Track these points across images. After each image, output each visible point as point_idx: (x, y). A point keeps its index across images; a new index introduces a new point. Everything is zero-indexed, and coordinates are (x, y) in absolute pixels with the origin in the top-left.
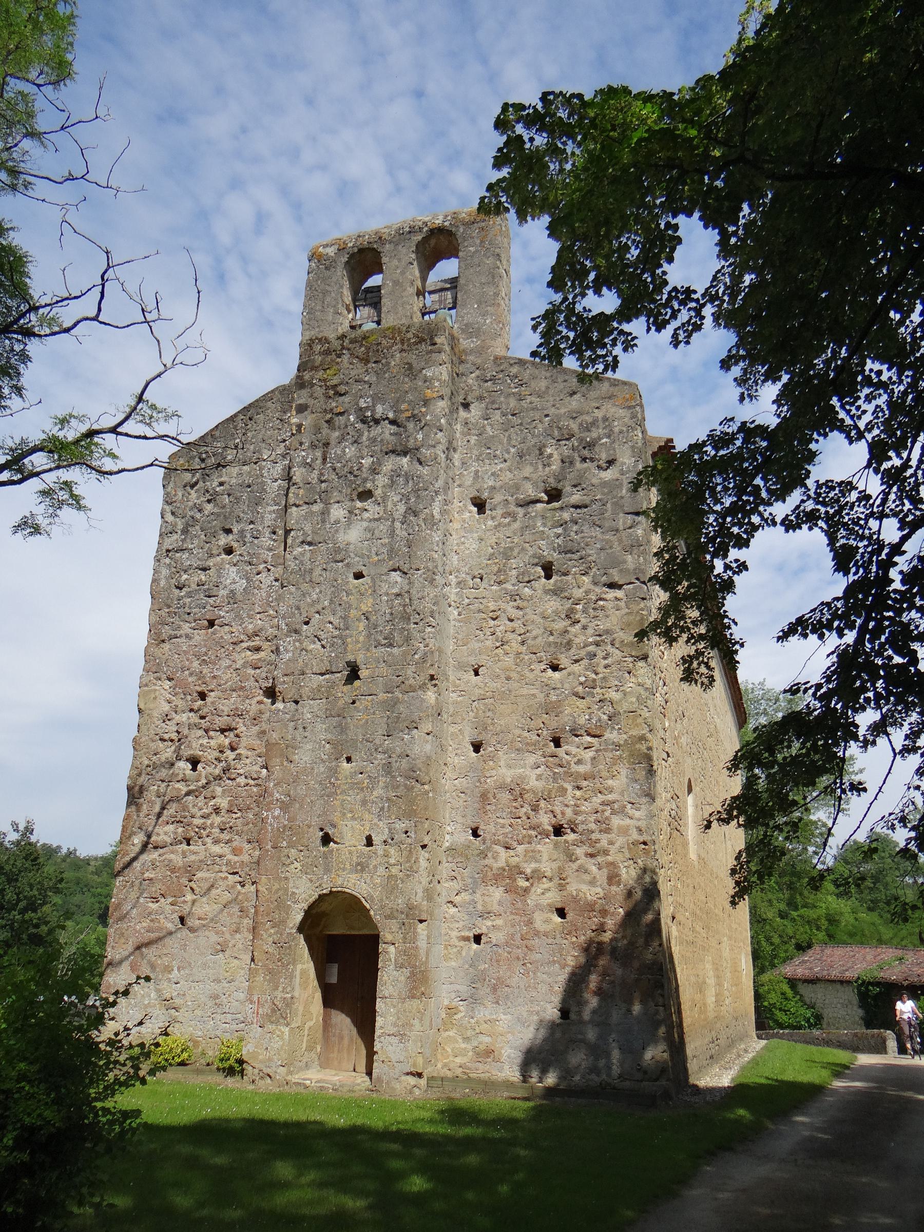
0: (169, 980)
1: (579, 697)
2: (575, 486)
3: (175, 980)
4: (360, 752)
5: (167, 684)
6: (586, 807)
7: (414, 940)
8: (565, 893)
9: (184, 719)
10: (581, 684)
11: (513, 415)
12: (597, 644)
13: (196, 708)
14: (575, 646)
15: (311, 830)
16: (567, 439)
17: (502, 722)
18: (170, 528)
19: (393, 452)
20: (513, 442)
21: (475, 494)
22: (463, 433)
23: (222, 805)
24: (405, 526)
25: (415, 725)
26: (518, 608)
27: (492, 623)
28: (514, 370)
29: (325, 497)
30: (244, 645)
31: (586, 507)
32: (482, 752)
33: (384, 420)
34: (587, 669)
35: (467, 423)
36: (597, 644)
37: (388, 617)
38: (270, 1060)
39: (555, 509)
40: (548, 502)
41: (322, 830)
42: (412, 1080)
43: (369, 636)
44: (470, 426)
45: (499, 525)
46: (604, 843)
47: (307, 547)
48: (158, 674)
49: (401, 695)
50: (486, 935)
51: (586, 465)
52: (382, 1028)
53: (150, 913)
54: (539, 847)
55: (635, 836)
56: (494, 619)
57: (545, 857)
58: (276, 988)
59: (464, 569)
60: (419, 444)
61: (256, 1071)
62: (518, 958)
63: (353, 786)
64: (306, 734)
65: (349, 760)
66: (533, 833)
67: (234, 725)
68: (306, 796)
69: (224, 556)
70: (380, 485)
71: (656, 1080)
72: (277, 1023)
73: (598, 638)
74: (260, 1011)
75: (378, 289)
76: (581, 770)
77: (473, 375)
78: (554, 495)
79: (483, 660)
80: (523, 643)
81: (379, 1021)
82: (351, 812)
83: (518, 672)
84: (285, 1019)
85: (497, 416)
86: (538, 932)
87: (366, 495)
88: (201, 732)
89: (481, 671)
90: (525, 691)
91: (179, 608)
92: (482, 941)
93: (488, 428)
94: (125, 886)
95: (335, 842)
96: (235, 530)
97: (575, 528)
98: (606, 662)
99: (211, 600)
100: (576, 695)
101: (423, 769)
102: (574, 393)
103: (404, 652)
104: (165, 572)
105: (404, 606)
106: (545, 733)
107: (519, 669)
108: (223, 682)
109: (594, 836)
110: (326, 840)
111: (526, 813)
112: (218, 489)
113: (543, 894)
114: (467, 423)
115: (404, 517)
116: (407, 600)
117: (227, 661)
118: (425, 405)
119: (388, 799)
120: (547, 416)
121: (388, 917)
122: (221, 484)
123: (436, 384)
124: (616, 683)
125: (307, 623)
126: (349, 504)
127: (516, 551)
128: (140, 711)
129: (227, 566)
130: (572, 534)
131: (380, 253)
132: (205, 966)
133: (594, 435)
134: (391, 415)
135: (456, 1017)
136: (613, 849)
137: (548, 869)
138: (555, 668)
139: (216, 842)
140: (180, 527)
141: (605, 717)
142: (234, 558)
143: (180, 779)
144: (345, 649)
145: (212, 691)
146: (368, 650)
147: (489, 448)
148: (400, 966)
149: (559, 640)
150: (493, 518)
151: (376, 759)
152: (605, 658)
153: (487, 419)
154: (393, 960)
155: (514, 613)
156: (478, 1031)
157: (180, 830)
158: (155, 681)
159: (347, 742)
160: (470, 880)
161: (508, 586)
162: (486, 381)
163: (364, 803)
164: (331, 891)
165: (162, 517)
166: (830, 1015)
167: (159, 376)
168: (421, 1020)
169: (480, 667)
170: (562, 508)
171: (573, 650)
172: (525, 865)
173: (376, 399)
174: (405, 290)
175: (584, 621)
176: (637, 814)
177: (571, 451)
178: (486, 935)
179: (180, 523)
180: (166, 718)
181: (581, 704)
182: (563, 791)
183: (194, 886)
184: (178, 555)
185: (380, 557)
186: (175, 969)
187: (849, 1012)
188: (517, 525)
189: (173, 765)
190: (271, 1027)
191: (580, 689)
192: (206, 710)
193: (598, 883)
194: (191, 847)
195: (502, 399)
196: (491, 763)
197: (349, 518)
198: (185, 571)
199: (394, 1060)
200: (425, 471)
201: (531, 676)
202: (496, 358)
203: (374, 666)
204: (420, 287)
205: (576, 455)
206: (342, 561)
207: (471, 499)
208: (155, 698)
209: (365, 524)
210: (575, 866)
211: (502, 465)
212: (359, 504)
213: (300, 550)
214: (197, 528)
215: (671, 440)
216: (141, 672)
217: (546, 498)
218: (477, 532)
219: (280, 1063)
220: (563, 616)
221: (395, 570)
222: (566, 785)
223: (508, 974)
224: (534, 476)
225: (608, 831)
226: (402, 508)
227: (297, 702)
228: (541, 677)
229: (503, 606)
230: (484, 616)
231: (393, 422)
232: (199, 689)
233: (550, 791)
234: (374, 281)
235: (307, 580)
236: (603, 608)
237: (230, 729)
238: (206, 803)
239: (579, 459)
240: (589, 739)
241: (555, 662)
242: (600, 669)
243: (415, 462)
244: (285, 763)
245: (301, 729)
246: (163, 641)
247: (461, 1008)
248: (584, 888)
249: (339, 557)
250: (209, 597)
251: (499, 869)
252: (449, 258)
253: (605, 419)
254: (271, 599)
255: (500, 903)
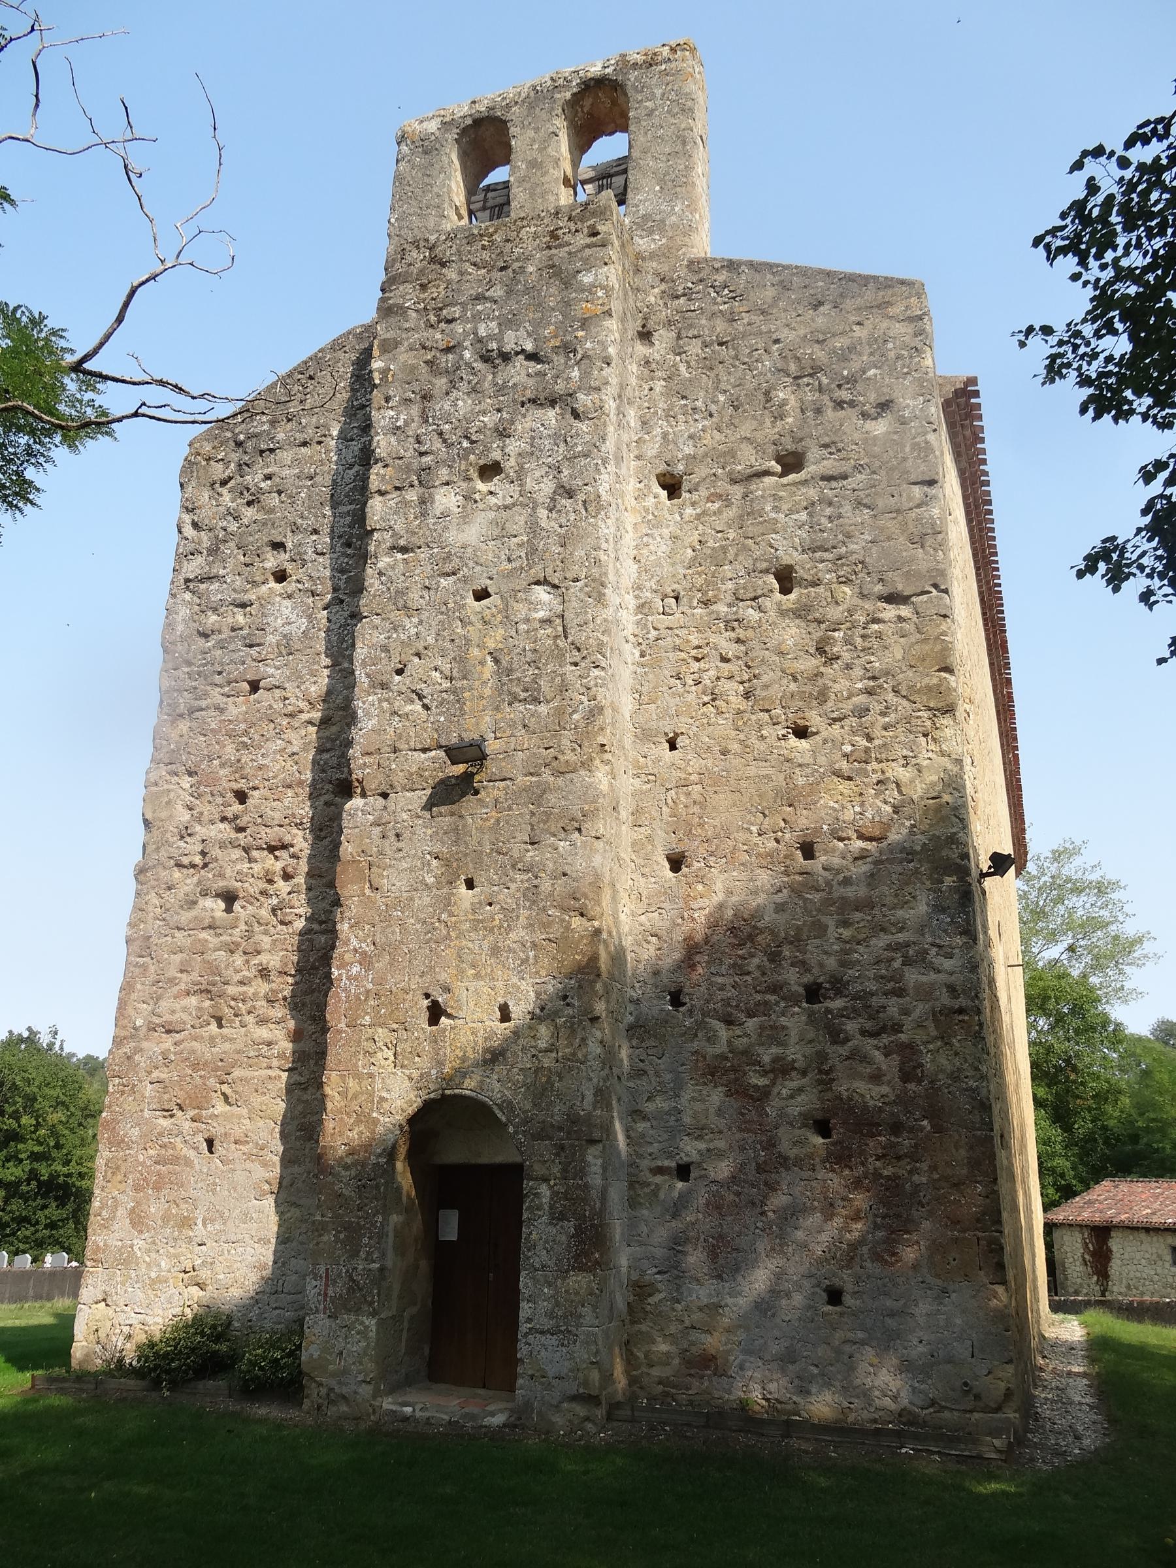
0: (190, 1240)
1: (843, 777)
2: (826, 446)
3: (199, 1240)
4: (487, 871)
5: (186, 782)
6: (860, 954)
7: (581, 1173)
8: (829, 1095)
9: (212, 834)
10: (846, 756)
11: (721, 344)
12: (870, 692)
13: (230, 815)
14: (833, 696)
15: (410, 997)
16: (810, 375)
17: (716, 822)
18: (191, 547)
19: (533, 401)
20: (723, 386)
21: (662, 468)
22: (641, 378)
23: (272, 963)
24: (554, 515)
25: (576, 825)
26: (738, 641)
27: (695, 666)
28: (721, 278)
29: (424, 478)
30: (305, 717)
31: (845, 477)
32: (684, 870)
33: (517, 353)
34: (853, 732)
35: (647, 362)
36: (870, 692)
37: (530, 656)
38: (345, 1372)
39: (794, 484)
40: (781, 476)
41: (427, 996)
42: (581, 1410)
43: (499, 690)
44: (654, 366)
45: (704, 513)
46: (893, 1010)
47: (399, 556)
48: (173, 767)
49: (552, 779)
50: (699, 1165)
51: (841, 414)
52: (529, 1320)
53: (160, 1134)
54: (784, 1021)
55: (945, 1000)
56: (697, 660)
57: (794, 1037)
58: (354, 1254)
59: (648, 585)
60: (572, 386)
61: (323, 1391)
62: (753, 1204)
63: (476, 925)
64: (400, 845)
65: (470, 884)
66: (772, 998)
67: (287, 839)
68: (402, 942)
69: (272, 584)
70: (512, 454)
71: (998, 1409)
72: (358, 1311)
73: (872, 683)
74: (330, 1292)
75: (506, 185)
76: (850, 895)
77: (656, 290)
78: (791, 462)
79: (682, 724)
80: (747, 695)
81: (525, 1309)
82: (474, 966)
83: (741, 742)
84: (371, 1304)
85: (694, 348)
86: (786, 1158)
87: (490, 470)
88: (237, 853)
89: (680, 743)
90: (752, 771)
91: (205, 665)
92: (692, 1175)
93: (683, 368)
94: (123, 1093)
95: (449, 1016)
96: (289, 545)
97: (828, 511)
98: (887, 719)
99: (253, 652)
100: (838, 774)
101: (591, 895)
102: (821, 303)
103: (557, 709)
104: (183, 612)
105: (556, 637)
106: (788, 836)
107: (742, 737)
108: (271, 774)
109: (875, 1001)
110: (436, 1012)
111: (759, 967)
112: (263, 485)
113: (792, 1097)
114: (647, 362)
115: (553, 500)
116: (560, 629)
117: (279, 742)
118: (583, 327)
119: (534, 945)
120: (777, 341)
121: (536, 1137)
122: (268, 477)
123: (600, 294)
124: (905, 752)
125: (400, 672)
126: (464, 485)
127: (732, 551)
128: (147, 823)
129: (278, 599)
130: (824, 521)
131: (505, 122)
132: (246, 1217)
133: (855, 366)
134: (529, 346)
135: (651, 1300)
136: (908, 1022)
137: (799, 1056)
138: (801, 732)
139: (262, 1021)
140: (206, 543)
141: (889, 809)
142: (290, 586)
143: (206, 925)
144: (461, 709)
145: (255, 788)
146: (497, 709)
147: (684, 397)
148: (558, 1217)
149: (808, 688)
150: (693, 504)
151: (513, 881)
152: (883, 714)
153: (679, 354)
154: (546, 1207)
155: (731, 649)
156: (687, 1323)
157: (208, 1003)
158: (168, 777)
159: (466, 855)
160: (669, 1076)
161: (722, 608)
162: (678, 297)
163: (495, 951)
164: (443, 1095)
165: (180, 532)
166: (1132, 1275)
167: (153, 277)
168: (595, 1307)
169: (677, 735)
170: (805, 482)
171: (830, 704)
172: (761, 1050)
173: (509, 322)
174: (547, 173)
175: (846, 656)
176: (948, 964)
177: (817, 394)
178: (699, 1165)
179: (205, 538)
180: (185, 833)
181: (844, 787)
182: (822, 930)
183: (228, 1091)
184: (203, 586)
185: (514, 564)
186: (199, 1222)
187: (1159, 1270)
188: (730, 513)
189: (195, 903)
190: (347, 1318)
191: (844, 765)
192: (246, 819)
193: (885, 1079)
194: (224, 1030)
195: (703, 322)
196: (700, 887)
197: (464, 507)
198: (215, 610)
199: (551, 1374)
200: (583, 426)
201: (760, 746)
202: (691, 262)
203: (508, 733)
204: (570, 173)
205: (826, 398)
206: (454, 574)
207: (658, 476)
208: (168, 803)
209: (492, 515)
210: (844, 1050)
211: (706, 423)
212: (481, 486)
213: (387, 560)
214: (232, 544)
215: (973, 381)
216: (148, 764)
217: (778, 469)
218: (668, 526)
219: (361, 1377)
220: (812, 650)
221: (538, 583)
222: (825, 919)
223: (737, 1229)
224: (759, 436)
225: (900, 993)
226: (548, 487)
227: (385, 796)
228: (777, 747)
229: (714, 638)
230: (683, 655)
231: (533, 357)
232: (235, 786)
233: (799, 929)
234: (498, 175)
235: (400, 605)
236: (879, 636)
237: (284, 847)
238: (247, 962)
239: (831, 404)
240: (860, 844)
241: (801, 722)
242: (878, 732)
243: (568, 416)
244: (368, 891)
245: (393, 838)
246: (181, 716)
247: (660, 1286)
248: (861, 1086)
249: (448, 568)
250: (251, 646)
251: (717, 1056)
252: (611, 134)
253: (872, 340)
254: (345, 645)
255: (720, 1112)
